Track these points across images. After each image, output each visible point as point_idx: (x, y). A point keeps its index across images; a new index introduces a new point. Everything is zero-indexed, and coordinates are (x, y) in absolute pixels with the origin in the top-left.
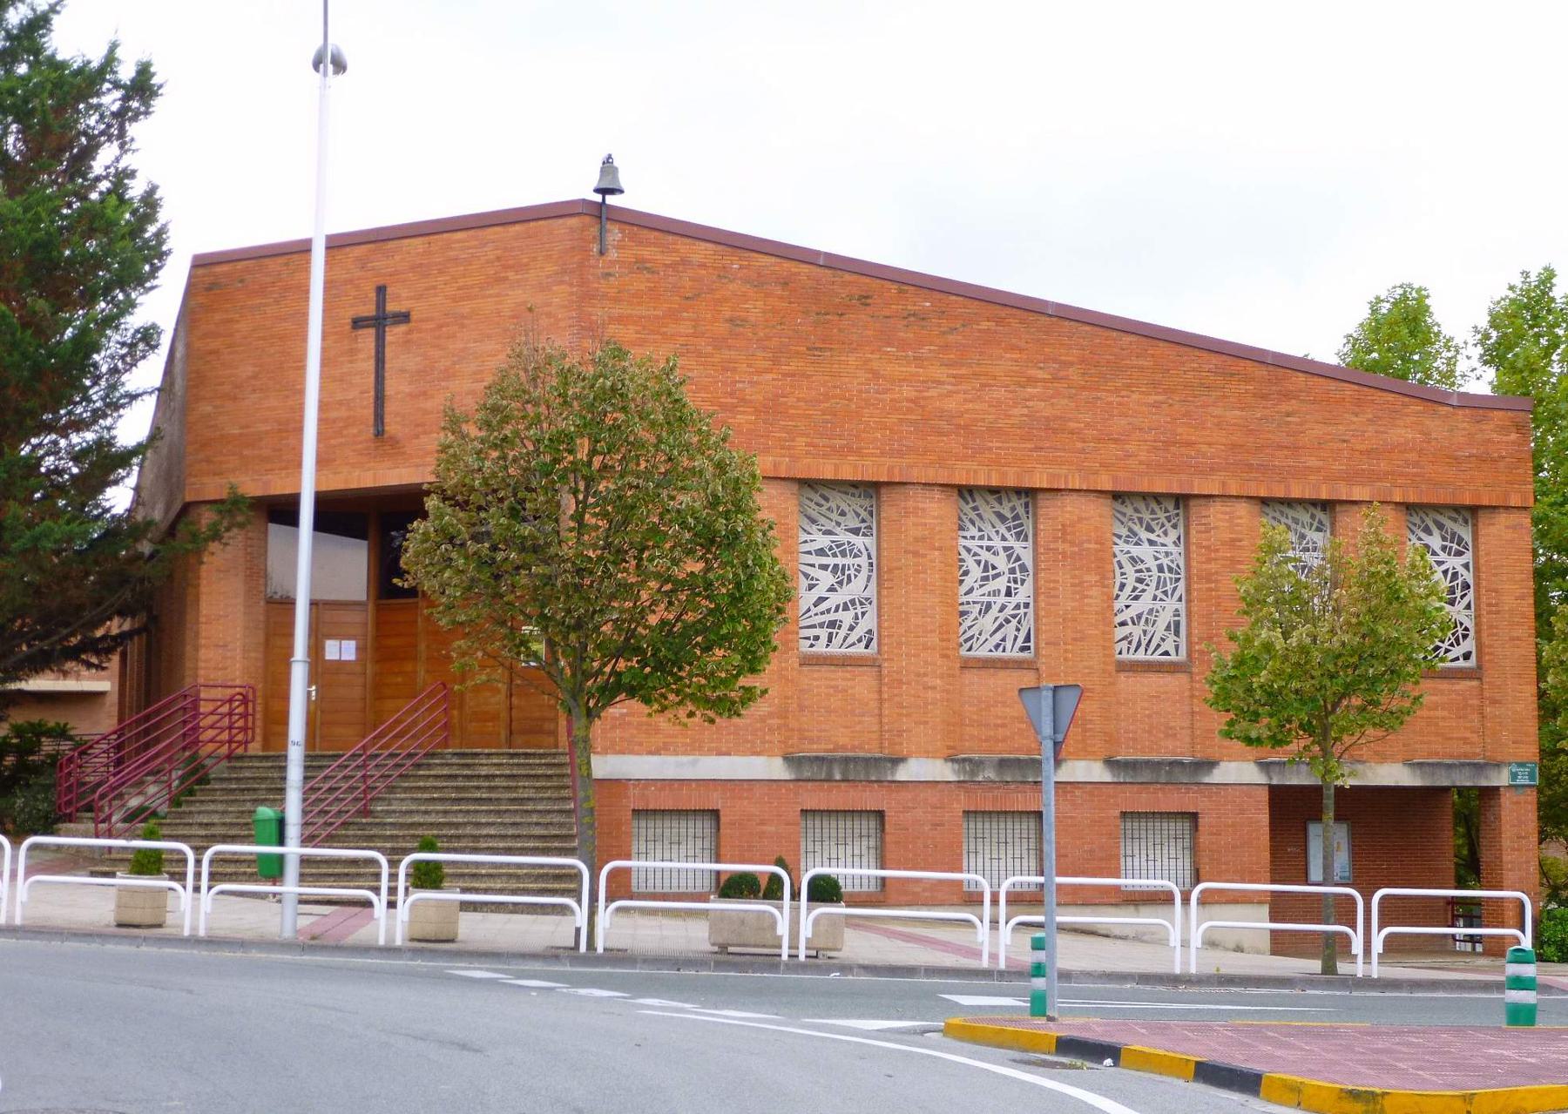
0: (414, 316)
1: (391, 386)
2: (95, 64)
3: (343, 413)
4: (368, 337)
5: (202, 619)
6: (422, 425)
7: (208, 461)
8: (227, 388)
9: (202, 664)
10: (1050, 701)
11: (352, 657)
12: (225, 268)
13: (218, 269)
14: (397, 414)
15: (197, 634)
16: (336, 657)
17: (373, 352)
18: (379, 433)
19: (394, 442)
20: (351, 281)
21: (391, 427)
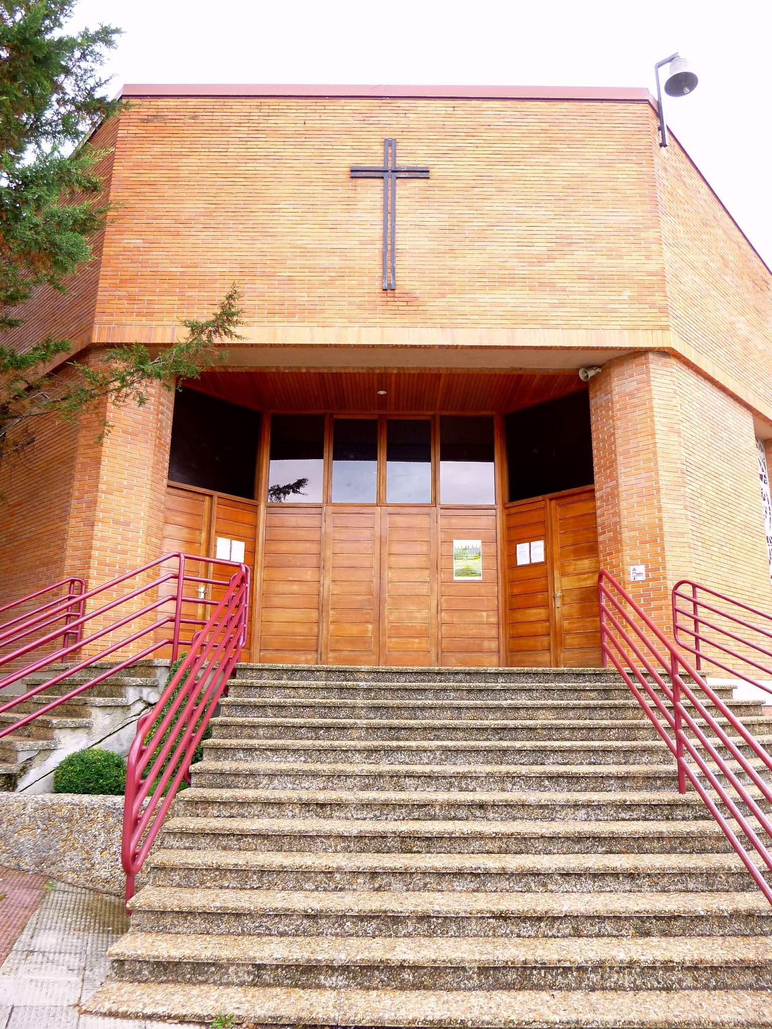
0: (434, 173)
1: (403, 241)
2: (109, 100)
3: (336, 261)
4: (373, 190)
5: (102, 487)
6: (451, 284)
7: (131, 299)
8: (165, 222)
9: (96, 543)
10: (311, 538)
11: (541, 559)
12: (172, 102)
13: (161, 103)
14: (413, 270)
15: (93, 504)
16: (527, 562)
17: (380, 204)
18: (389, 289)
19: (410, 299)
20: (349, 132)
21: (405, 281)
